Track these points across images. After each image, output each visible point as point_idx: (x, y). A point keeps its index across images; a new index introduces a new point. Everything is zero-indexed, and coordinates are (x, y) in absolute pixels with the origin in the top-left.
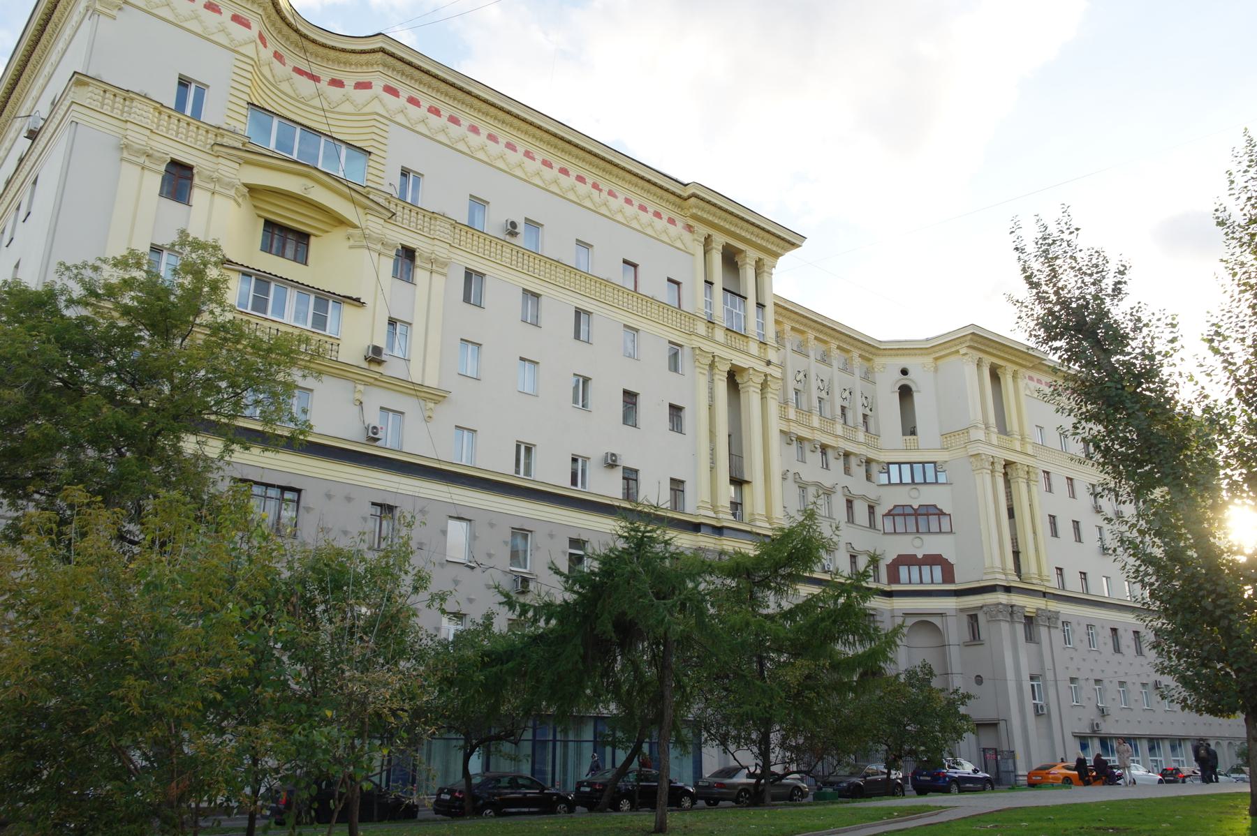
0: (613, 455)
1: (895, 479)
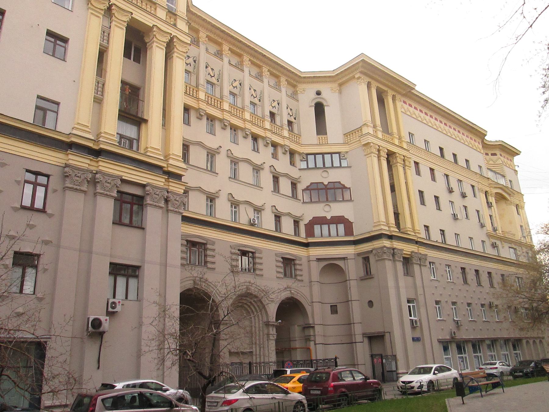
1: (312, 165)
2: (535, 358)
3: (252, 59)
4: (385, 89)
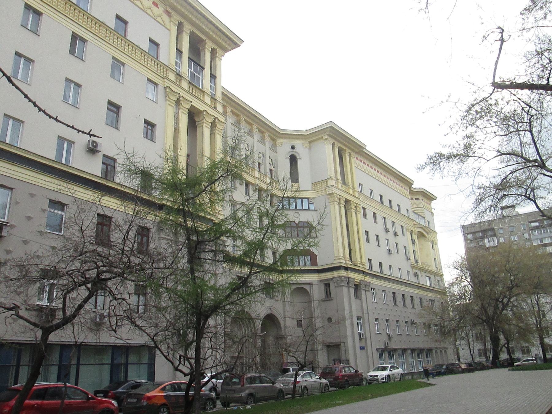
2: (446, 363)
4: (344, 148)
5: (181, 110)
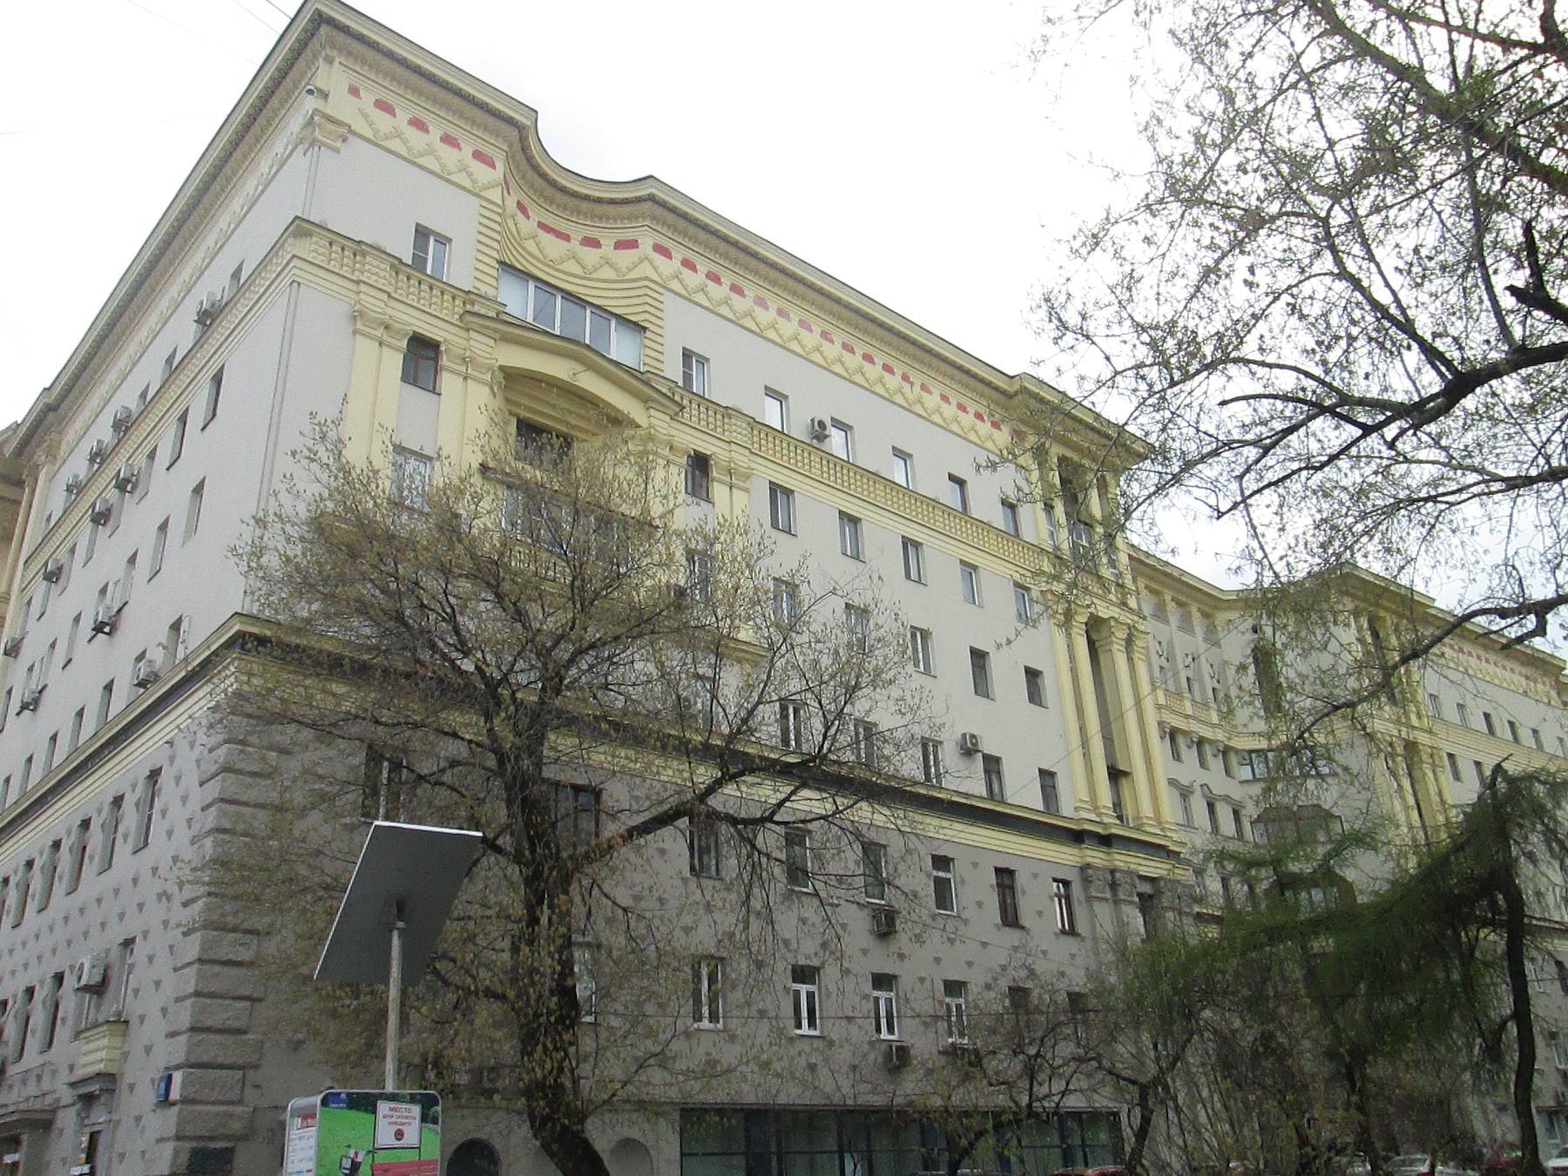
0: (973, 736)
3: (1203, 607)
5: (1075, 630)
